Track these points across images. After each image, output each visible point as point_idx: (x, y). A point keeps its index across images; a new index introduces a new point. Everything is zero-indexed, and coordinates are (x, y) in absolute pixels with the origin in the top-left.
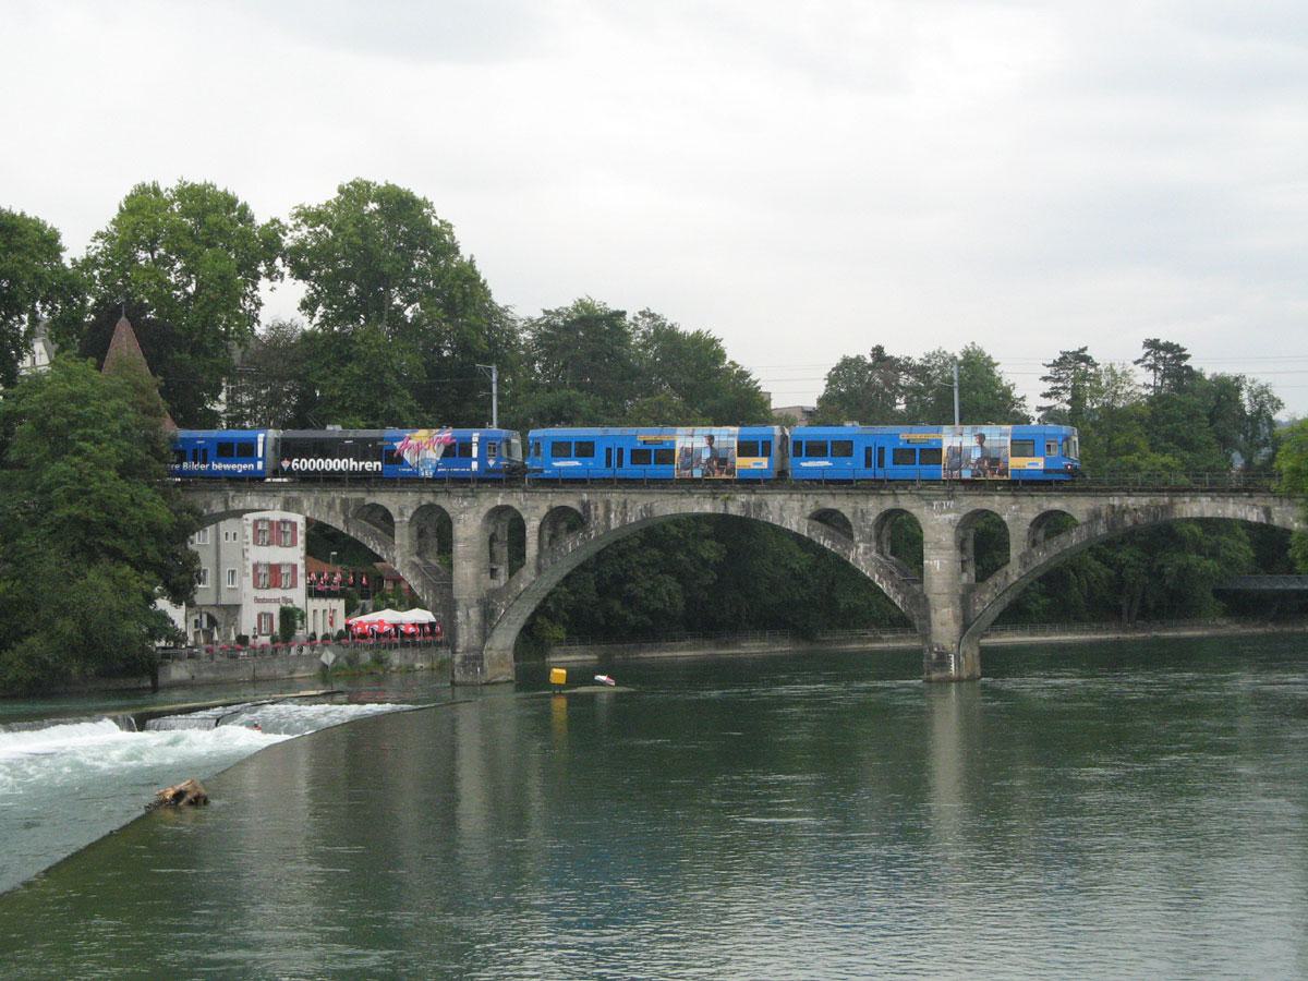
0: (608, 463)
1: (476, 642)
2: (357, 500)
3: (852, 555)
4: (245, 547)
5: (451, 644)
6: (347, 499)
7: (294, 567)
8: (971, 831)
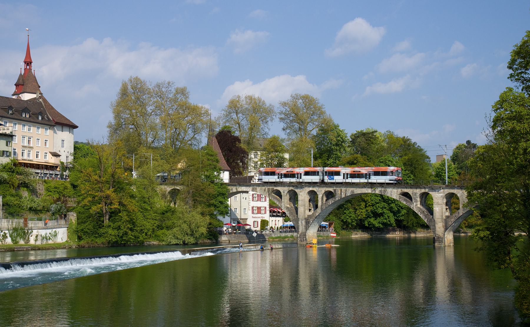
0: (344, 178)
1: (304, 231)
2: (272, 188)
3: (412, 206)
4: (249, 202)
5: (297, 231)
6: (269, 188)
7: (265, 208)
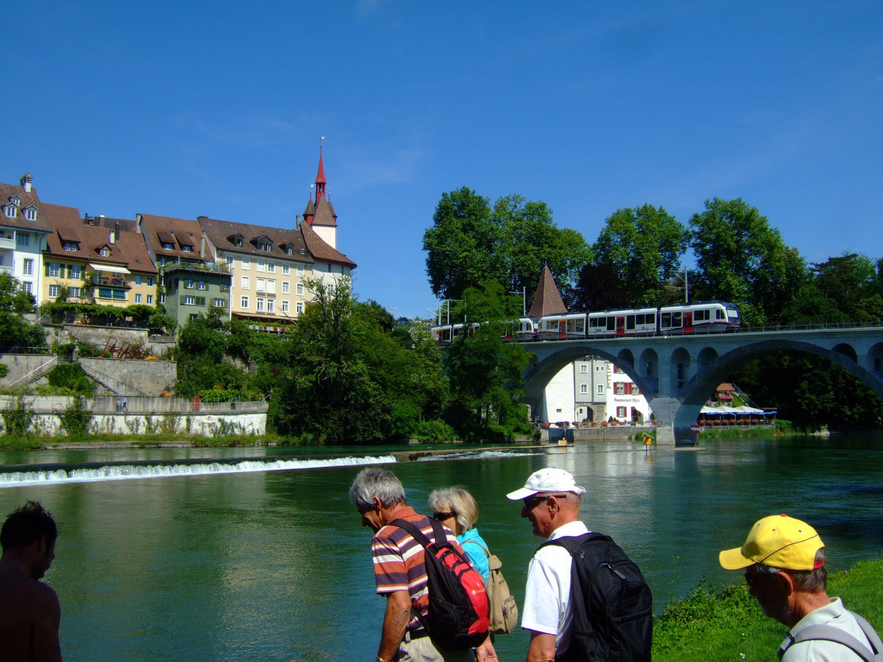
4: (609, 374)
8: (156, 471)
